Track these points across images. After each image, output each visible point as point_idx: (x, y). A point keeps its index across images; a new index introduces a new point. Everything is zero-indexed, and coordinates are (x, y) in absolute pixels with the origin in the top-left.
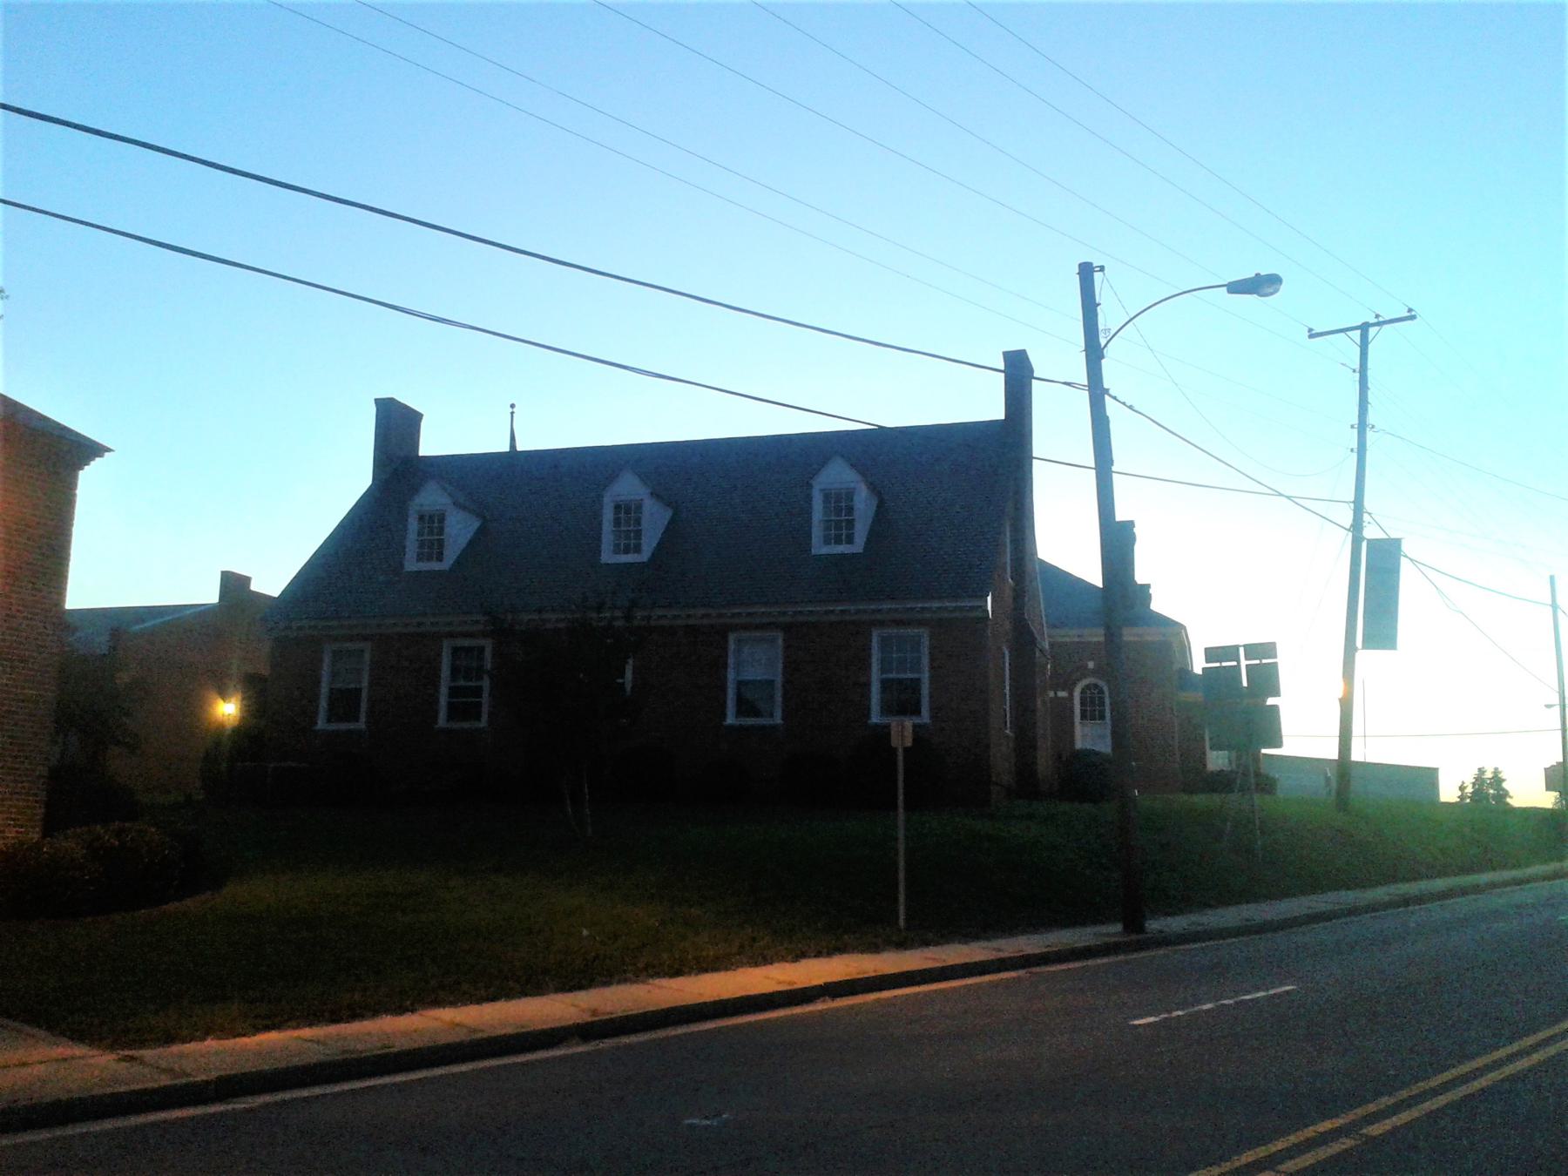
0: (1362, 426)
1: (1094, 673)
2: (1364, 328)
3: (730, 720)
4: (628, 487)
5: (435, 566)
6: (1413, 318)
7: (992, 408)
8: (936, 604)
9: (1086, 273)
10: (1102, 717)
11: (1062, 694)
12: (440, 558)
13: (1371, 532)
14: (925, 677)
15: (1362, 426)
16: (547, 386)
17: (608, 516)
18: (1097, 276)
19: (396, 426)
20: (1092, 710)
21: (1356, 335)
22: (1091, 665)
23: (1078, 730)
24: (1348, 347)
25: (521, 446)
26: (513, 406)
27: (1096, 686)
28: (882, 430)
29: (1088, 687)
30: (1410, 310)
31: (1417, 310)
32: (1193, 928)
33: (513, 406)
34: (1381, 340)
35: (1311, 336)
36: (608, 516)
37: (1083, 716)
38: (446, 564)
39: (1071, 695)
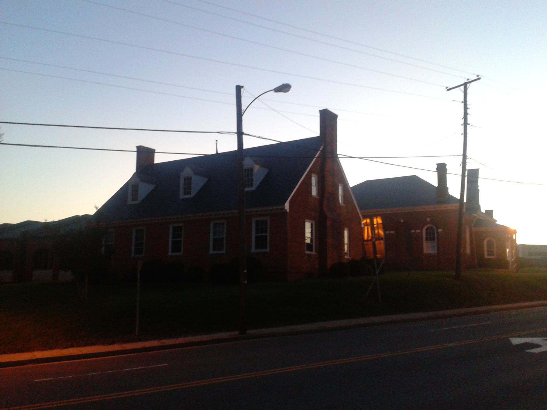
0: (466, 124)
1: (431, 222)
2: (465, 85)
3: (170, 254)
4: (187, 172)
5: (188, 196)
6: (479, 79)
7: (313, 130)
8: (275, 208)
9: (239, 89)
10: (434, 239)
11: (418, 231)
12: (252, 186)
13: (468, 167)
14: (268, 234)
15: (466, 124)
16: (195, 134)
17: (182, 181)
18: (242, 90)
19: (145, 155)
20: (430, 237)
21: (462, 87)
22: (428, 220)
23: (425, 244)
24: (459, 94)
25: (219, 152)
26: (217, 141)
27: (432, 228)
28: (281, 145)
29: (428, 228)
30: (478, 76)
31: (478, 74)
32: (123, 349)
33: (217, 141)
34: (470, 87)
35: (448, 90)
36: (182, 181)
37: (427, 239)
38: (191, 196)
39: (421, 232)
